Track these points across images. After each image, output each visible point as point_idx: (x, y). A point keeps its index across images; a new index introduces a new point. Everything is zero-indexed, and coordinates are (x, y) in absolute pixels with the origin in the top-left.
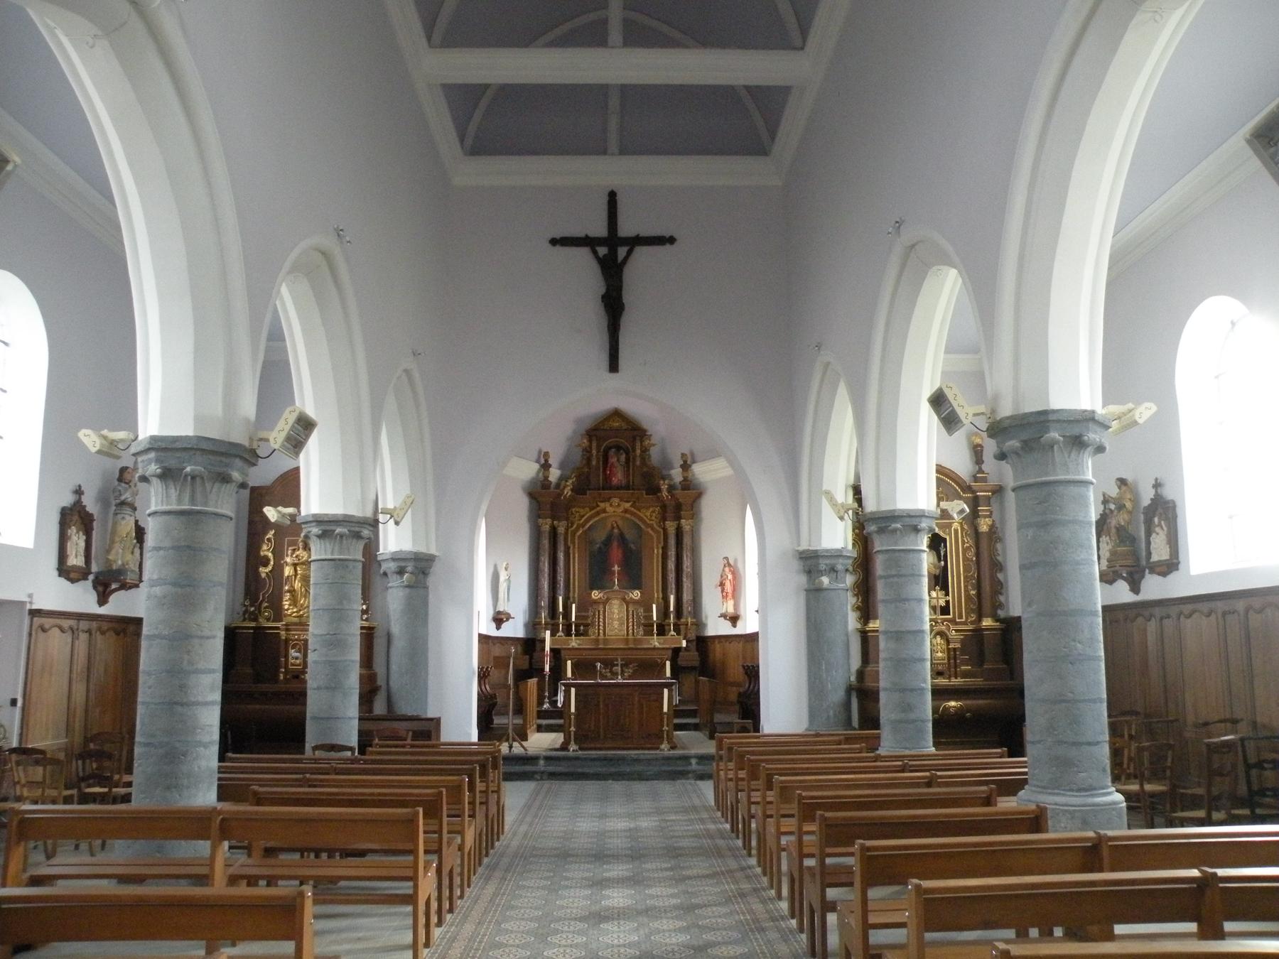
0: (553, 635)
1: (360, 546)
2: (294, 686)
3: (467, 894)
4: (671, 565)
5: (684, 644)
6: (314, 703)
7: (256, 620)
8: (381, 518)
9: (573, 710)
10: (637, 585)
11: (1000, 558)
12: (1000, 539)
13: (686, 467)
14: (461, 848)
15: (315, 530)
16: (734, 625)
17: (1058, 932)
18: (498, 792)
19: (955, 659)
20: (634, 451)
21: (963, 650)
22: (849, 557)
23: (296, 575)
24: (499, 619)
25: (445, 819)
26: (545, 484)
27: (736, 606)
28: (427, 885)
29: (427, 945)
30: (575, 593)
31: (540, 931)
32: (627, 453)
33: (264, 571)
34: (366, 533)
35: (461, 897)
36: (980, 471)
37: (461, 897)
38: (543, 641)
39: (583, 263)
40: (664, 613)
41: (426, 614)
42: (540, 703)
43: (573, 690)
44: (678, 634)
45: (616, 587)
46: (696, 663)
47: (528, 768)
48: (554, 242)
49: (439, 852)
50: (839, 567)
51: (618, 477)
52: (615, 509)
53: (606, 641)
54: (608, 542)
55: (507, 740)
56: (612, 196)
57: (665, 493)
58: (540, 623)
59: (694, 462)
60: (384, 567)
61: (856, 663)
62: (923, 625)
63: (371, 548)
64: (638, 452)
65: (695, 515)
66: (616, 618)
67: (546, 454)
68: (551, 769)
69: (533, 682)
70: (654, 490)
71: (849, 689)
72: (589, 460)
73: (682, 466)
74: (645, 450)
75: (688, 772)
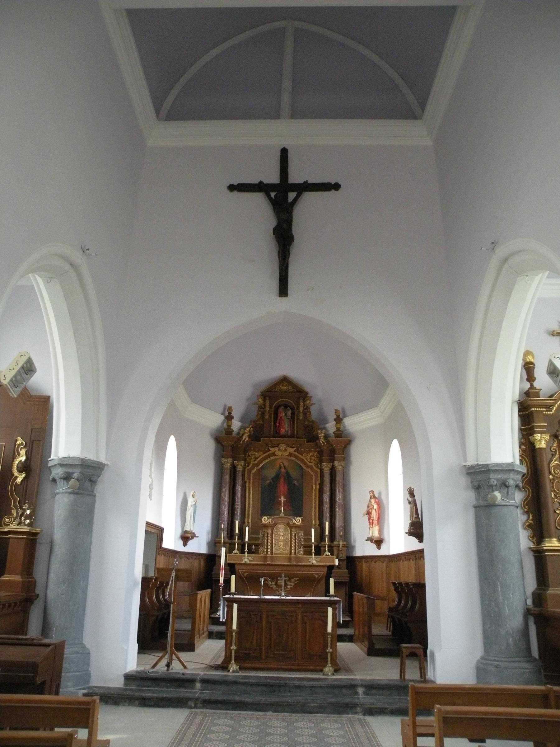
4: (326, 498)
5: (337, 562)
10: (298, 513)
13: (338, 420)
16: (379, 548)
20: (298, 408)
22: (518, 472)
24: (186, 538)
26: (229, 431)
27: (381, 531)
30: (249, 519)
31: (235, 733)
32: (293, 409)
39: (259, 208)
41: (91, 523)
43: (235, 606)
44: (332, 554)
45: (282, 515)
47: (183, 692)
48: (232, 188)
50: (511, 483)
51: (285, 428)
52: (282, 453)
53: (273, 558)
54: (276, 478)
56: (284, 153)
57: (322, 440)
58: (220, 542)
59: (345, 416)
61: (531, 585)
64: (301, 409)
65: (346, 459)
66: (281, 540)
67: (230, 409)
68: (207, 694)
70: (313, 438)
71: (528, 613)
72: (263, 414)
73: (335, 420)
74: (307, 409)
75: (355, 706)
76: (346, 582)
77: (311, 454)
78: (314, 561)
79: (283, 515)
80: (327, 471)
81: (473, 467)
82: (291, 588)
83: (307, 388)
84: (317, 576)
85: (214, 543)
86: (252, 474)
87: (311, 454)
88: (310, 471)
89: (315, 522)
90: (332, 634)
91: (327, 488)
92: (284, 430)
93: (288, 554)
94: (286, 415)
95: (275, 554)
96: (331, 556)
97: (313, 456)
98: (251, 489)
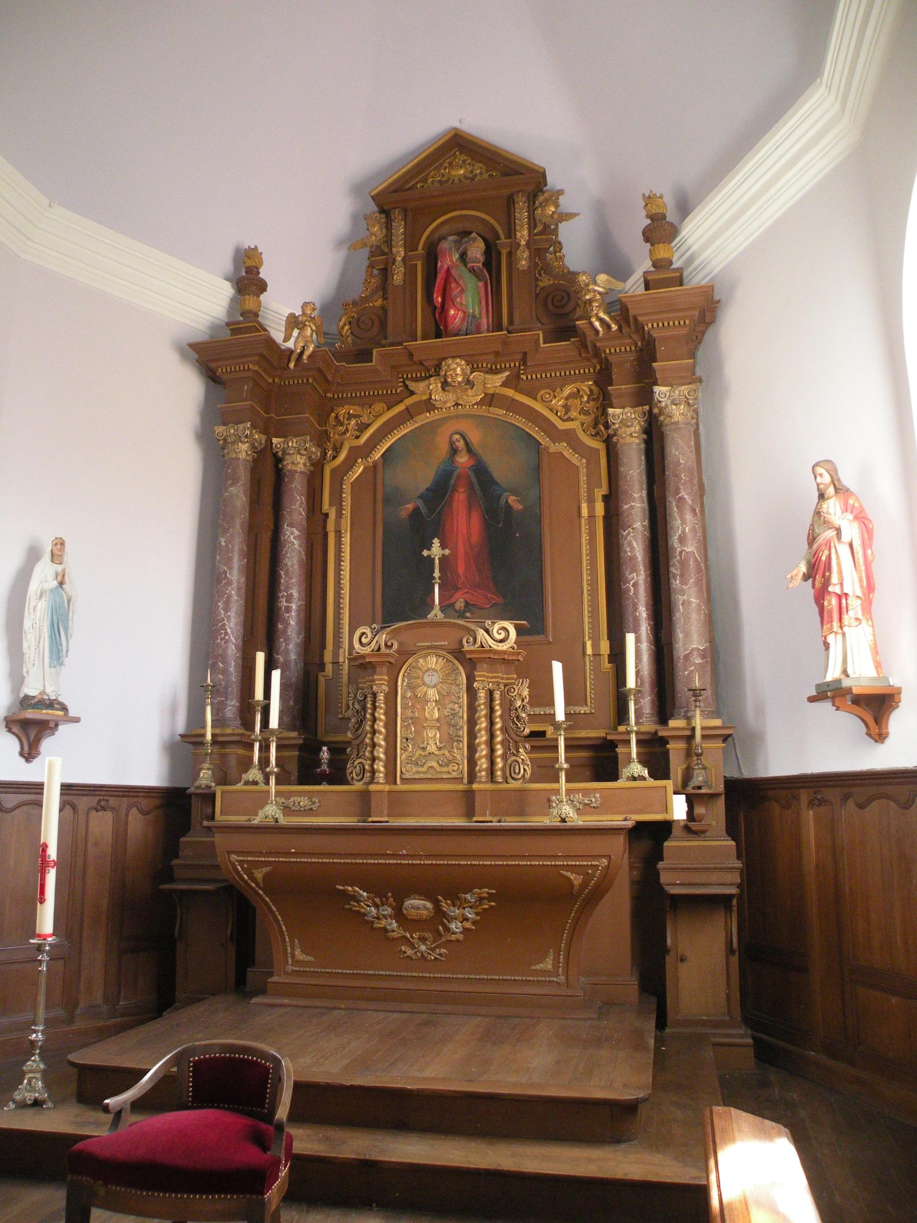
4: (635, 545)
5: (679, 808)
17: (425, 553)
20: (511, 232)
45: (436, 614)
51: (468, 301)
54: (439, 492)
59: (685, 208)
64: (523, 235)
72: (385, 272)
74: (545, 239)
76: (730, 897)
77: (567, 391)
78: (567, 810)
79: (440, 616)
82: (466, 931)
84: (576, 879)
86: (347, 488)
87: (567, 391)
88: (568, 453)
89: (596, 646)
91: (636, 505)
92: (460, 315)
93: (459, 780)
94: (463, 256)
95: (405, 781)
96: (651, 782)
97: (577, 394)
98: (347, 539)
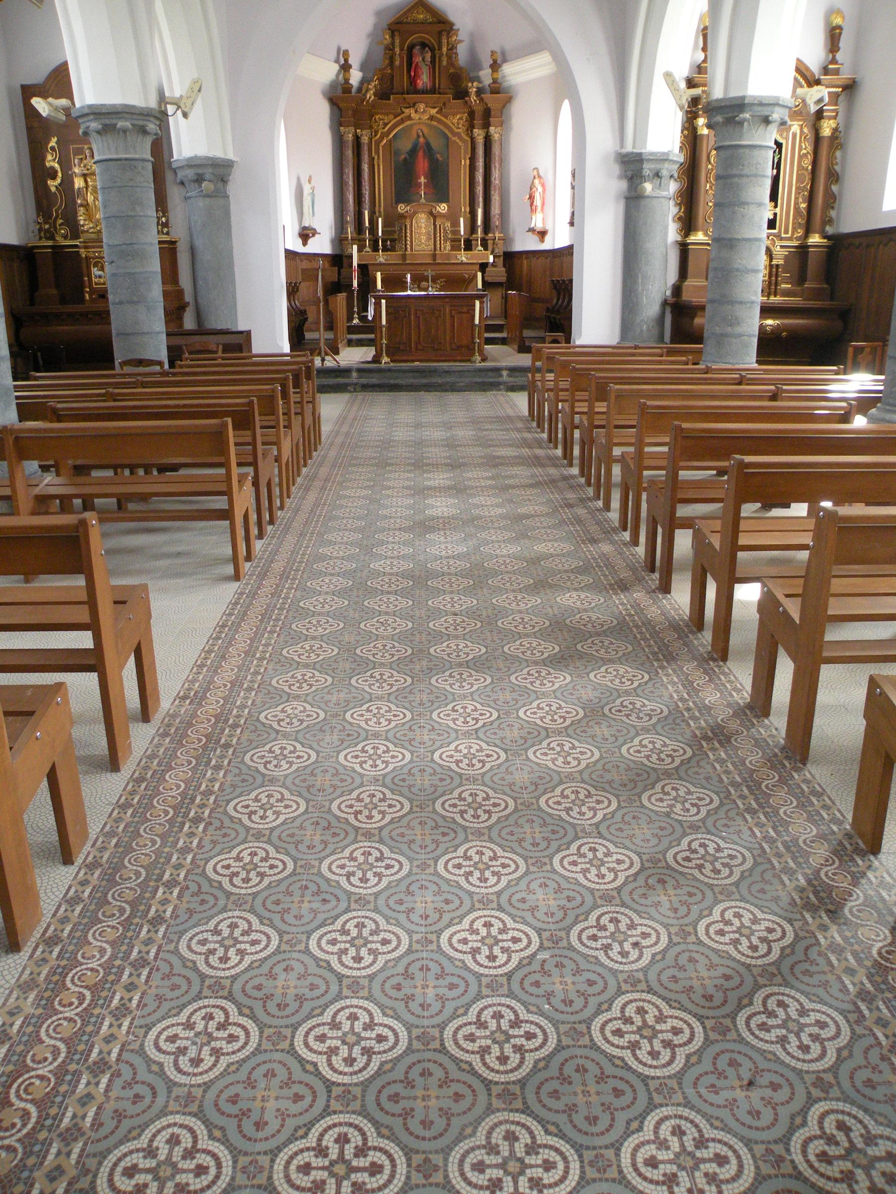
0: (360, 250)
1: (148, 142)
2: (100, 305)
3: (287, 505)
4: (480, 178)
5: (491, 259)
6: (119, 319)
7: (52, 238)
8: (170, 109)
9: (384, 322)
10: (444, 198)
11: (837, 168)
12: (841, 146)
13: (495, 66)
14: (277, 459)
15: (94, 125)
18: (313, 402)
19: (777, 276)
20: (440, 48)
21: (786, 267)
22: (674, 162)
23: (87, 187)
24: (305, 235)
25: (258, 431)
26: (346, 87)
28: (244, 499)
29: (248, 558)
30: (381, 207)
32: (432, 50)
33: (53, 184)
34: (152, 127)
35: (282, 508)
36: (834, 61)
37: (282, 508)
38: (351, 257)
40: (473, 228)
42: (350, 319)
44: (486, 249)
45: (423, 200)
46: (504, 279)
47: (340, 380)
49: (254, 464)
51: (424, 80)
52: (421, 116)
54: (413, 151)
55: (319, 354)
57: (473, 98)
59: (505, 61)
60: (181, 174)
61: (672, 277)
62: (762, 233)
63: (161, 147)
64: (445, 49)
68: (363, 381)
69: (341, 297)
70: (461, 94)
71: (665, 303)
73: (491, 66)
74: (452, 48)
75: (499, 384)
80: (480, 140)
81: (627, 155)
83: (452, 18)
85: (340, 240)
90: (479, 326)
